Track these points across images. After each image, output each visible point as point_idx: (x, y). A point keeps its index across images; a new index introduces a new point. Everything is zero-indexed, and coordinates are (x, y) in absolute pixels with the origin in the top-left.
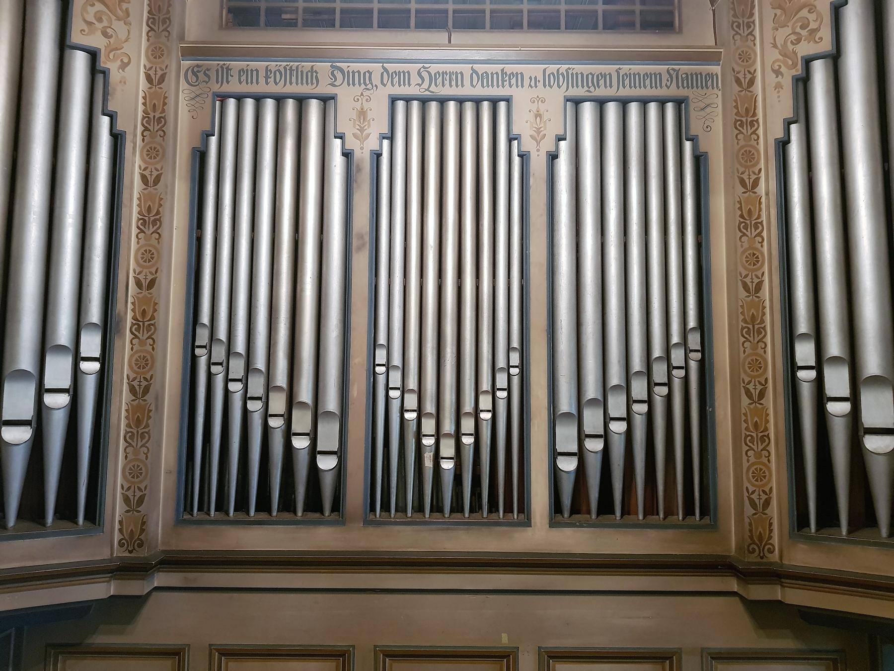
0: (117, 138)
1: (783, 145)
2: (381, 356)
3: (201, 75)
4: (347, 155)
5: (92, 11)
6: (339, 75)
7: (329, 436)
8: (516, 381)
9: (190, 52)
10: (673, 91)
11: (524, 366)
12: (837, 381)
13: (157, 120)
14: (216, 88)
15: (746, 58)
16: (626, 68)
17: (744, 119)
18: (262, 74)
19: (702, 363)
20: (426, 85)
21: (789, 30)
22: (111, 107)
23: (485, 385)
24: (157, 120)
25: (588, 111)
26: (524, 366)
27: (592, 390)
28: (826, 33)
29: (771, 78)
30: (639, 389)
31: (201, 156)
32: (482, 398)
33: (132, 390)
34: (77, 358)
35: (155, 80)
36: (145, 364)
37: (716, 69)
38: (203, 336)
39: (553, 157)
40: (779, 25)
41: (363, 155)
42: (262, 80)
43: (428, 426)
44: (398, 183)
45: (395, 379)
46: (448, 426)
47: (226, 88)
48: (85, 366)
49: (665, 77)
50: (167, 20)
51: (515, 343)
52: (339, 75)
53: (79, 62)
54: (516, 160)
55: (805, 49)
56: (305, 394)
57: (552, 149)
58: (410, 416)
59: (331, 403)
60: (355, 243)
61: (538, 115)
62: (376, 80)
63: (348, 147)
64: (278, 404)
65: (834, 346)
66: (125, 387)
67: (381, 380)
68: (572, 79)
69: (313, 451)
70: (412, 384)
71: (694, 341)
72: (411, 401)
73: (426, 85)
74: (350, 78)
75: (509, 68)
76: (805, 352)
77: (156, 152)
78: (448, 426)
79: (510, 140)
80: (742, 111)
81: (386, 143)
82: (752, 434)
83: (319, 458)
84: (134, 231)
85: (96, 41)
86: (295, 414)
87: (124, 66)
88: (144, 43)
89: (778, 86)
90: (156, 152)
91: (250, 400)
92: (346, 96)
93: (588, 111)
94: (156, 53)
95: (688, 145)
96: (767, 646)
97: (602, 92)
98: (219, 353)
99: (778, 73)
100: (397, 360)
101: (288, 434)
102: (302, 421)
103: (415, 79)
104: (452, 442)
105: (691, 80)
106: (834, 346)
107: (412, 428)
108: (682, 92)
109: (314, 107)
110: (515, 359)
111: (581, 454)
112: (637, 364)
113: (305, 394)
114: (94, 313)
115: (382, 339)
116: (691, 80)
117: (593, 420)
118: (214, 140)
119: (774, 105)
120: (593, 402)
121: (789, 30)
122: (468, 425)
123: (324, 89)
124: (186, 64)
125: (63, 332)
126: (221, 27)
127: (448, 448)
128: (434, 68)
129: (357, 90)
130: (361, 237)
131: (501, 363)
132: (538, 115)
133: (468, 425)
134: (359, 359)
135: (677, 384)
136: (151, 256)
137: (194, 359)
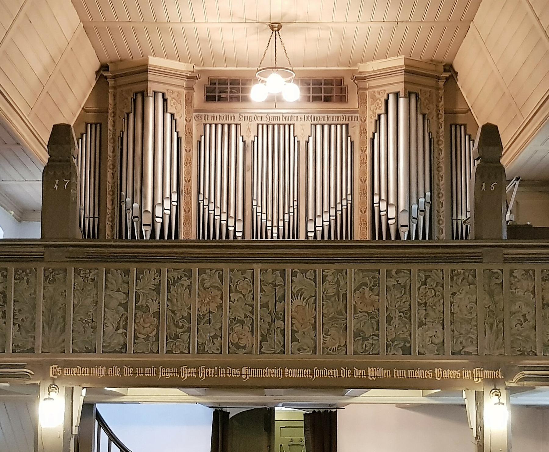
0: (179, 139)
1: (373, 140)
2: (255, 203)
3: (199, 118)
4: (244, 142)
5: (172, 102)
6: (241, 117)
7: (239, 227)
8: (296, 210)
9: (196, 111)
10: (344, 122)
11: (298, 206)
12: (383, 206)
13: (189, 133)
14: (204, 122)
15: (364, 113)
16: (329, 115)
17: (363, 131)
18: (218, 117)
19: (351, 204)
20: (268, 120)
21: (374, 106)
22: (178, 130)
23: (286, 211)
24: (189, 133)
25: (319, 128)
26: (298, 206)
27: (319, 213)
28: (383, 107)
29: (370, 120)
30: (333, 212)
31: (200, 142)
32: (285, 215)
33: (185, 211)
34: (171, 201)
35: (188, 121)
36: (188, 203)
37: (357, 115)
38: (201, 197)
39: (307, 142)
40: (372, 104)
41: (249, 142)
42: (218, 119)
43: (269, 224)
44: (260, 150)
45: (259, 210)
46: (275, 224)
47: (207, 122)
48: (173, 203)
49: (342, 117)
50: (191, 102)
51: (296, 199)
52: (241, 117)
53: (168, 116)
54: (296, 143)
55: (378, 112)
56: (232, 214)
57: (307, 140)
58: (264, 221)
59: (240, 217)
60: (247, 169)
61: (303, 129)
62: (253, 119)
63: (244, 140)
64: (224, 217)
65: (383, 197)
66: (183, 210)
67: (255, 210)
68: (314, 119)
69: (235, 231)
70: (264, 211)
71: (349, 198)
72: (264, 216)
73: (268, 120)
74: (246, 118)
75: (294, 115)
76: (376, 199)
77: (189, 142)
78: (275, 224)
79: (294, 137)
80: (362, 129)
81: (256, 138)
82: (362, 222)
83: (237, 233)
84: (184, 165)
85: (172, 112)
86: (229, 220)
87: (180, 118)
88: (185, 110)
89: (371, 122)
90: (189, 142)
91: (217, 214)
92: (244, 123)
93: (319, 128)
94: (188, 112)
95: (349, 138)
96: (173, 80)
97: (322, 122)
98: (206, 202)
99: (371, 118)
100: (260, 204)
101: (227, 226)
102: (231, 222)
103: (265, 118)
104: (276, 228)
105: (349, 118)
106: (383, 197)
107: (264, 224)
108: (347, 122)
109: (233, 127)
110: (296, 204)
111: (315, 232)
112: (332, 205)
113: (232, 214)
114: (175, 189)
115: (255, 198)
116: (349, 118)
117: (319, 222)
118: (203, 137)
119: (371, 128)
120: (319, 216)
121: (374, 106)
122: (281, 223)
123: (237, 122)
124: (195, 114)
125: (167, 194)
126: (204, 102)
127: (275, 230)
128: (270, 115)
129: (247, 122)
130: (249, 167)
131: (291, 205)
132: (303, 129)
133: (281, 223)
134: (248, 203)
135: (344, 211)
136: (189, 173)
137: (199, 203)
